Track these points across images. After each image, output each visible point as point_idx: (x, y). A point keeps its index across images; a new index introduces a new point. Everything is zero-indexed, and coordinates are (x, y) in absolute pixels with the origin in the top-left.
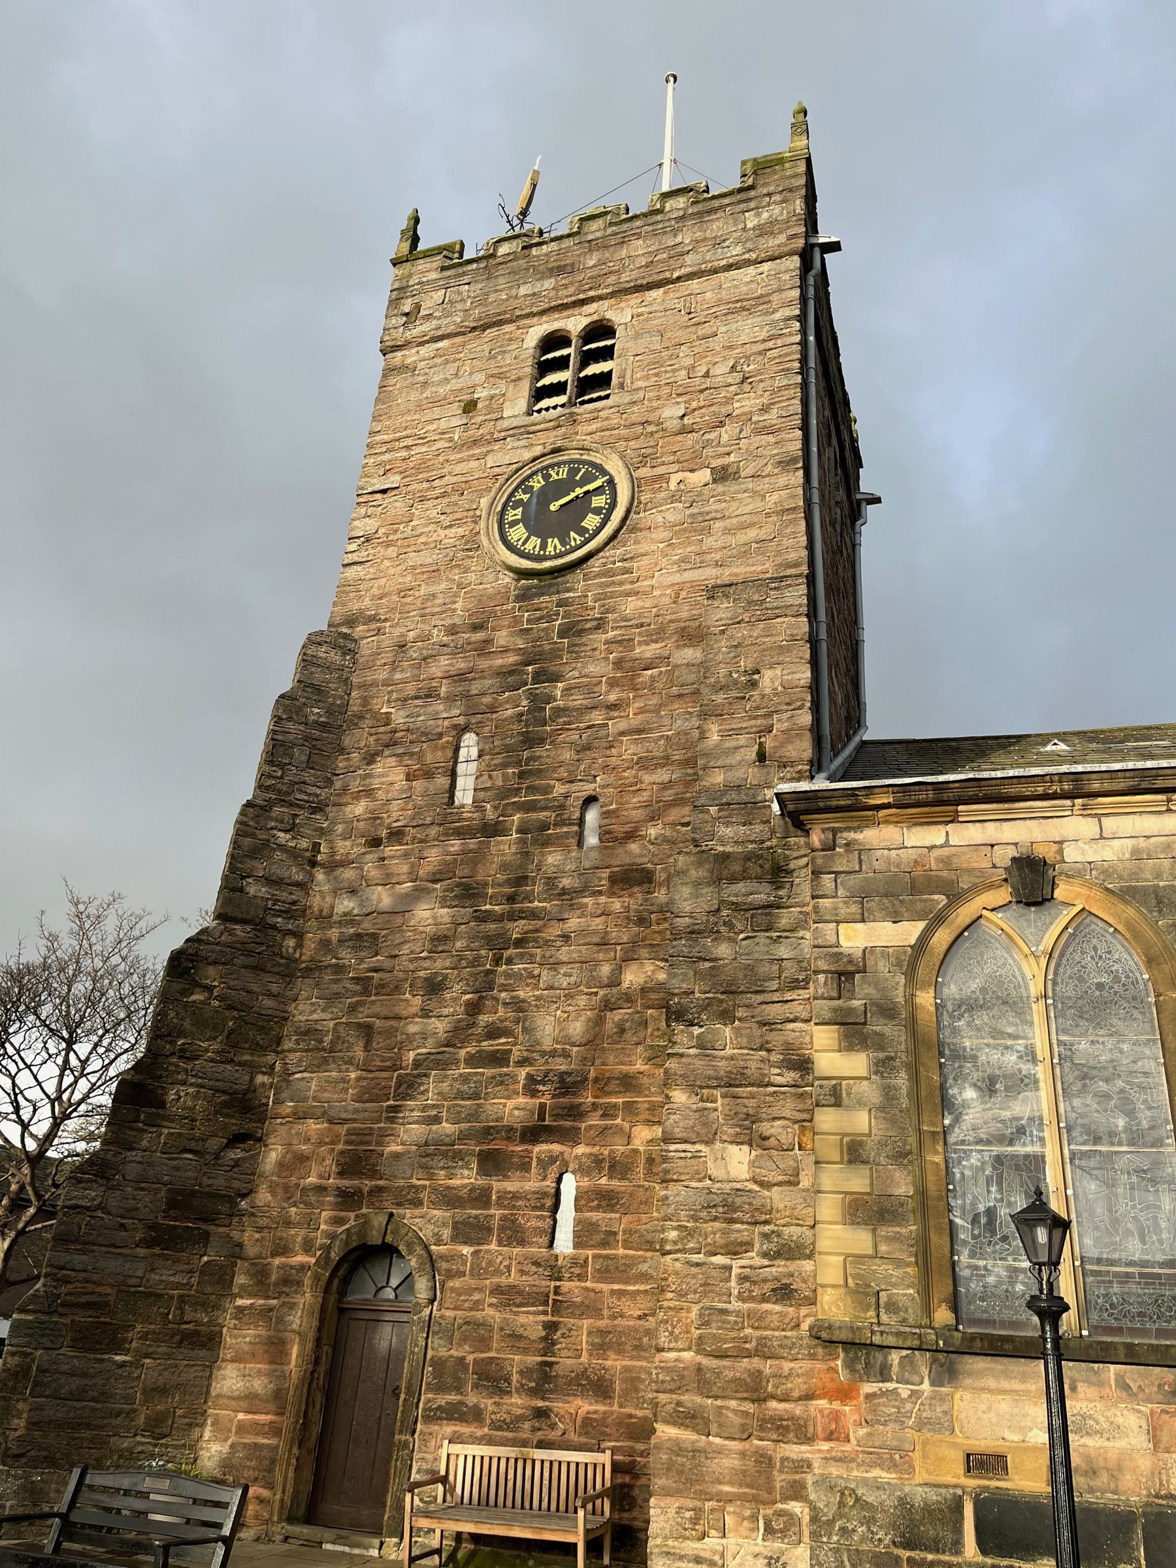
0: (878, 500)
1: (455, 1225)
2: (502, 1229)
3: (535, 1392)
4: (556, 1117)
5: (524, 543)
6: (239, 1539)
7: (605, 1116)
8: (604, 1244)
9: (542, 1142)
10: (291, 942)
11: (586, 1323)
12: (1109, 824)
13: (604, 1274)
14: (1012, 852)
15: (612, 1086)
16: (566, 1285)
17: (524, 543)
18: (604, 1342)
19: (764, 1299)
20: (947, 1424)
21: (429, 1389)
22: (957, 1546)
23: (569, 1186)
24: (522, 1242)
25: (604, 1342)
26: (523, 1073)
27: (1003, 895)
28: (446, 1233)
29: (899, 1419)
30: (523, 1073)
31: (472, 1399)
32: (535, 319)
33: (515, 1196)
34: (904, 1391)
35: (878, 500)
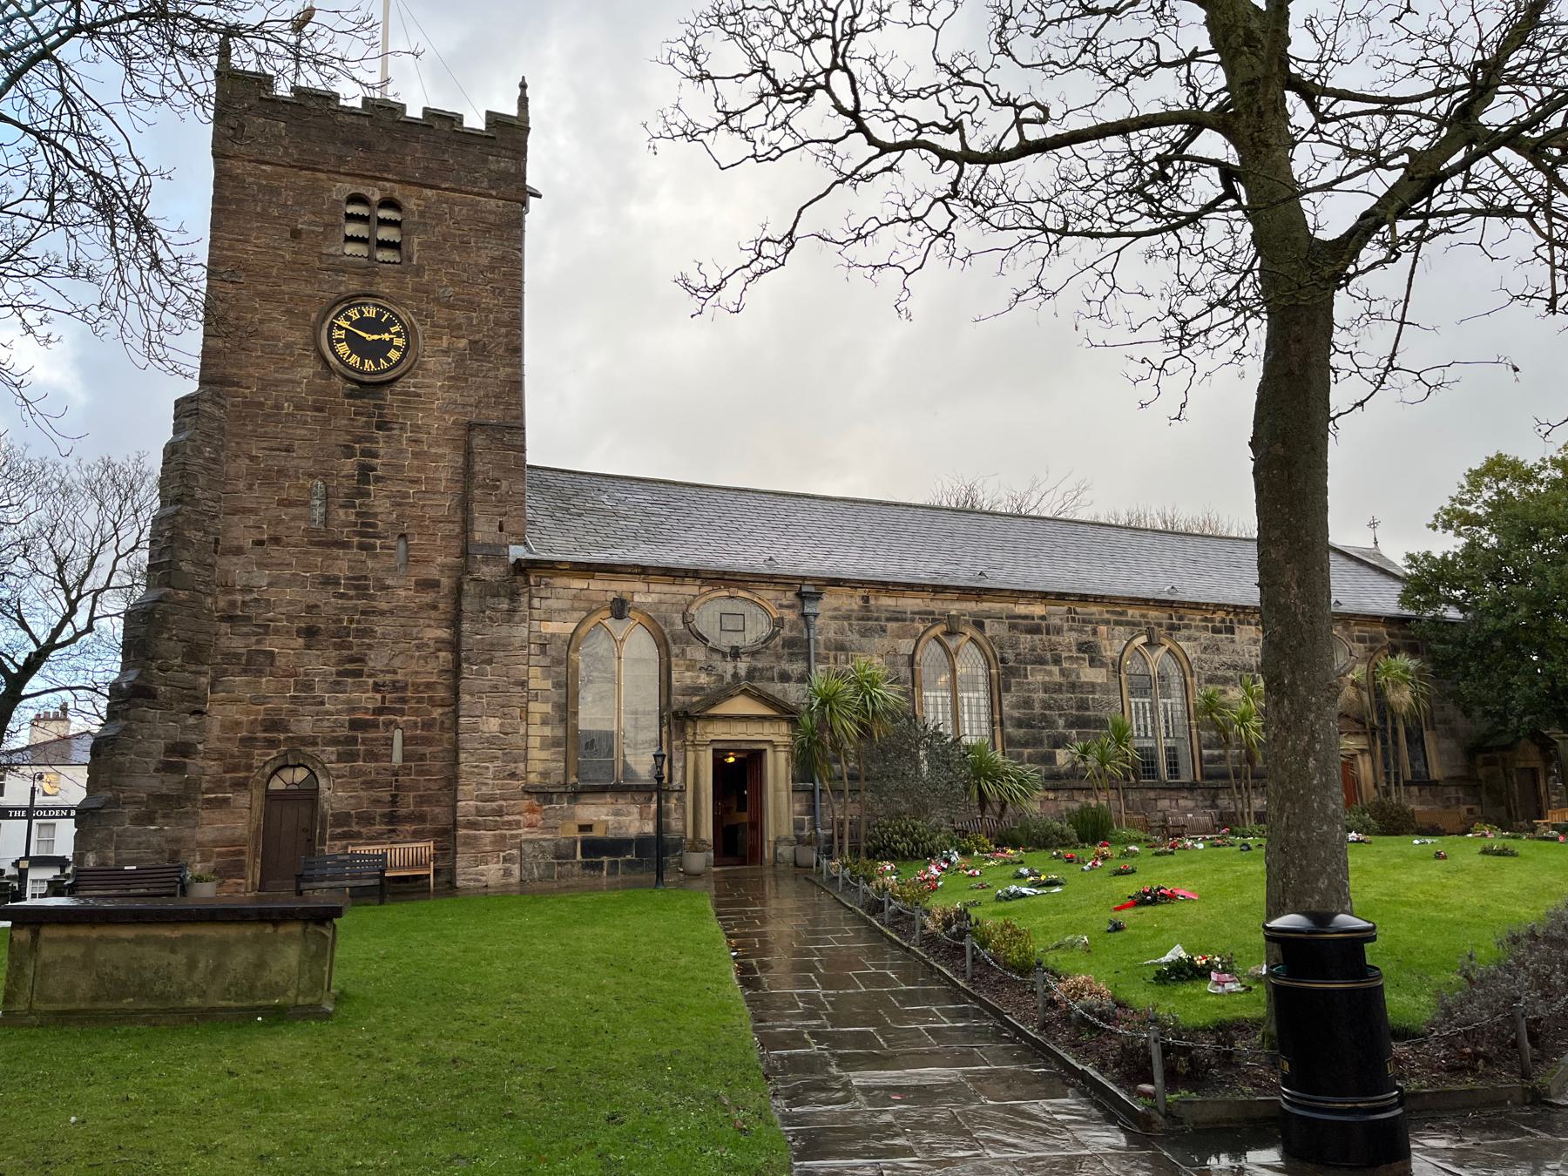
0: (540, 196)
1: (339, 754)
2: (365, 755)
3: (390, 823)
4: (392, 702)
5: (349, 357)
6: (1256, 642)
7: (418, 702)
8: (421, 760)
9: (1444, 1129)
10: (209, 600)
11: (412, 794)
12: (652, 587)
13: (420, 773)
14: (614, 595)
15: (421, 688)
16: (400, 778)
17: (349, 357)
18: (421, 800)
19: (504, 779)
20: (572, 817)
21: (332, 826)
22: (574, 857)
23: (398, 735)
24: (376, 761)
25: (421, 800)
26: (371, 681)
27: (608, 613)
28: (334, 758)
29: (555, 817)
30: (371, 681)
31: (355, 828)
32: (342, 177)
33: (372, 740)
34: (558, 807)
35: (540, 196)
